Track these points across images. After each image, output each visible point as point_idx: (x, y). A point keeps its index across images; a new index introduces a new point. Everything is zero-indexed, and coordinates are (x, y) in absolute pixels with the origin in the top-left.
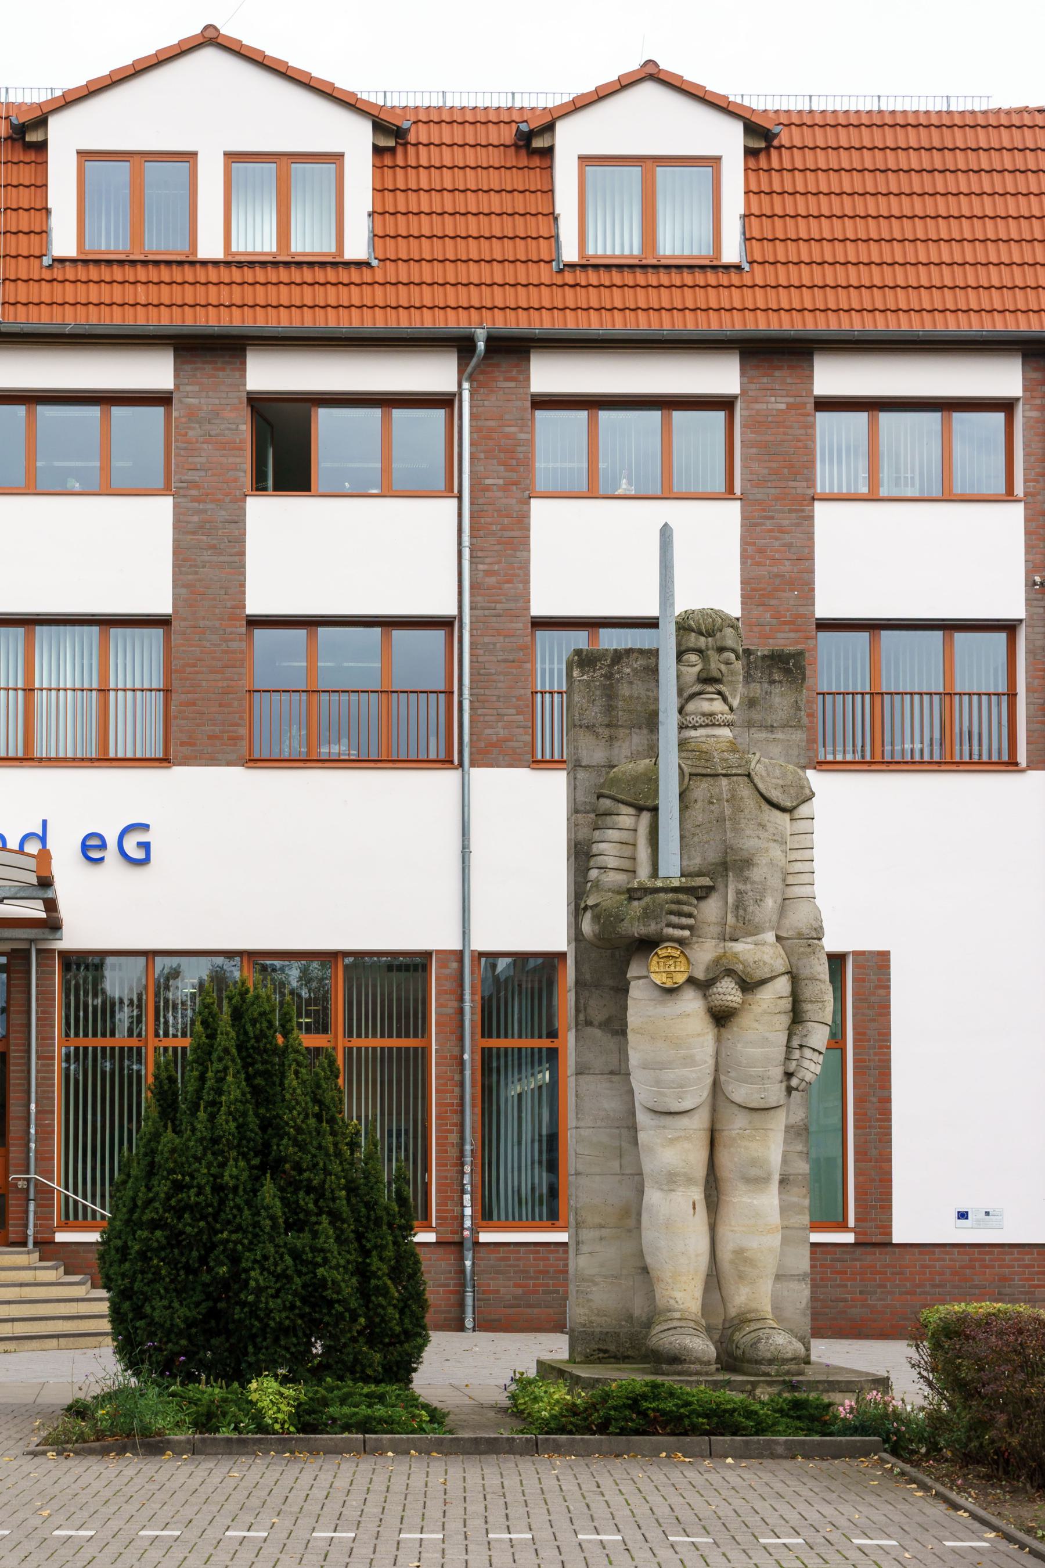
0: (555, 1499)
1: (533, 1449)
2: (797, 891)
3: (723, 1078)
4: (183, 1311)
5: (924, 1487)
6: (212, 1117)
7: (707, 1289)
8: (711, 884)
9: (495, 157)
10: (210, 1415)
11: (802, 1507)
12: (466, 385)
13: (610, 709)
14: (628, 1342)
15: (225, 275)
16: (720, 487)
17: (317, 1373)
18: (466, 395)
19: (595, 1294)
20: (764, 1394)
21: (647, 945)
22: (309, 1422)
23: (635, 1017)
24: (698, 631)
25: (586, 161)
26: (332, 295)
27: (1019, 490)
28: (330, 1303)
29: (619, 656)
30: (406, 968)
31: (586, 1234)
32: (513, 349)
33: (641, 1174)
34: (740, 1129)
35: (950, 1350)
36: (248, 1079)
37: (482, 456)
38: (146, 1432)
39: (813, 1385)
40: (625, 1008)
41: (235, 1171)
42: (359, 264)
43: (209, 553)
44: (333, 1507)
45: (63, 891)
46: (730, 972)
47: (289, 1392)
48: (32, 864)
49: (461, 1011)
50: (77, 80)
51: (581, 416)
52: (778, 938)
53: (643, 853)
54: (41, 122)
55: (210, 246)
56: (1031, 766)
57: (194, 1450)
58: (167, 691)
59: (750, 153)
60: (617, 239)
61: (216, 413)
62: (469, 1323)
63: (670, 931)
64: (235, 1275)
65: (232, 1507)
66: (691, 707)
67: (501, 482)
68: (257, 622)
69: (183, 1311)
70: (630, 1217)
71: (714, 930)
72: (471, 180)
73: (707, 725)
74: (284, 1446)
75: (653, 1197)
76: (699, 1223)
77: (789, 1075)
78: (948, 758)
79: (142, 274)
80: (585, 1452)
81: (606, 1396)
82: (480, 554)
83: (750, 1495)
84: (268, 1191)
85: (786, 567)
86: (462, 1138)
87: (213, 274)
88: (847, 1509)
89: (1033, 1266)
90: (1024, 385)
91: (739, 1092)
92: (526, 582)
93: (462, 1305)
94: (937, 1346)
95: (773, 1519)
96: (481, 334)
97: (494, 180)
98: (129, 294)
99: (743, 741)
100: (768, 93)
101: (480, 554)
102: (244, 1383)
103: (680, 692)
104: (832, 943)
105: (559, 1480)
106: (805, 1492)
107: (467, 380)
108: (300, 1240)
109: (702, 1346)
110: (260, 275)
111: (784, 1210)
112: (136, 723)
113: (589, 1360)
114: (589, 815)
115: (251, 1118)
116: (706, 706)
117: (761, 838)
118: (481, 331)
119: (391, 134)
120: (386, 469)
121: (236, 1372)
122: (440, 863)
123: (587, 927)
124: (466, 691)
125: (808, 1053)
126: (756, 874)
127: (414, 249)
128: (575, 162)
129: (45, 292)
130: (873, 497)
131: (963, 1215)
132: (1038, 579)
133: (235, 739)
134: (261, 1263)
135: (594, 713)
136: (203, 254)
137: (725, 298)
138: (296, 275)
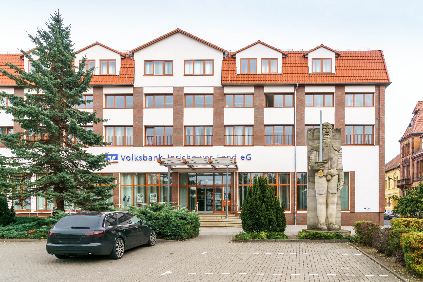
0: (301, 248)
1: (299, 241)
4: (252, 222)
5: (354, 247)
6: (256, 195)
7: (326, 219)
9: (300, 58)
10: (255, 237)
11: (336, 250)
13: (313, 137)
14: (315, 227)
15: (261, 76)
16: (332, 105)
17: (270, 231)
19: (310, 220)
20: (333, 233)
21: (318, 171)
22: (269, 238)
24: (325, 126)
25: (313, 59)
26: (276, 79)
27: (375, 105)
28: (272, 221)
29: (314, 129)
30: (287, 174)
31: (309, 211)
32: (302, 86)
35: (358, 227)
36: (261, 190)
38: (245, 239)
39: (340, 232)
41: (259, 203)
42: (280, 74)
43: (259, 115)
44: (269, 250)
45: (238, 164)
46: (329, 174)
47: (266, 234)
48: (233, 160)
50: (240, 48)
51: (363, 95)
53: (317, 157)
54: (235, 55)
55: (259, 72)
57: (252, 242)
58: (253, 135)
59: (336, 57)
60: (317, 70)
61: (260, 96)
64: (259, 217)
65: (255, 250)
68: (265, 126)
69: (252, 222)
71: (327, 168)
72: (296, 62)
74: (265, 241)
75: (318, 206)
76: (325, 210)
77: (338, 189)
78: (364, 144)
79: (249, 76)
80: (307, 242)
81: (310, 234)
83: (329, 248)
84: (263, 205)
85: (341, 117)
87: (259, 76)
88: (342, 250)
91: (331, 191)
92: (304, 119)
93: (294, 221)
94: (356, 227)
95: (331, 251)
96: (298, 84)
97: (300, 62)
98: (248, 79)
99: (332, 141)
100: (339, 48)
102: (260, 233)
104: (345, 170)
105: (303, 245)
106: (337, 247)
108: (268, 212)
109: (325, 227)
110: (266, 76)
111: (337, 208)
112: (249, 140)
113: (309, 229)
114: (310, 152)
115: (261, 195)
116: (326, 136)
117: (335, 155)
119: (285, 56)
120: (244, 104)
121: (259, 231)
122: (291, 160)
123: (309, 168)
126: (333, 160)
127: (288, 72)
128: (261, 59)
129: (236, 79)
130: (354, 107)
131: (365, 209)
133: (262, 142)
134: (262, 216)
135: (311, 138)
136: (258, 73)
137: (333, 78)
138: (271, 76)
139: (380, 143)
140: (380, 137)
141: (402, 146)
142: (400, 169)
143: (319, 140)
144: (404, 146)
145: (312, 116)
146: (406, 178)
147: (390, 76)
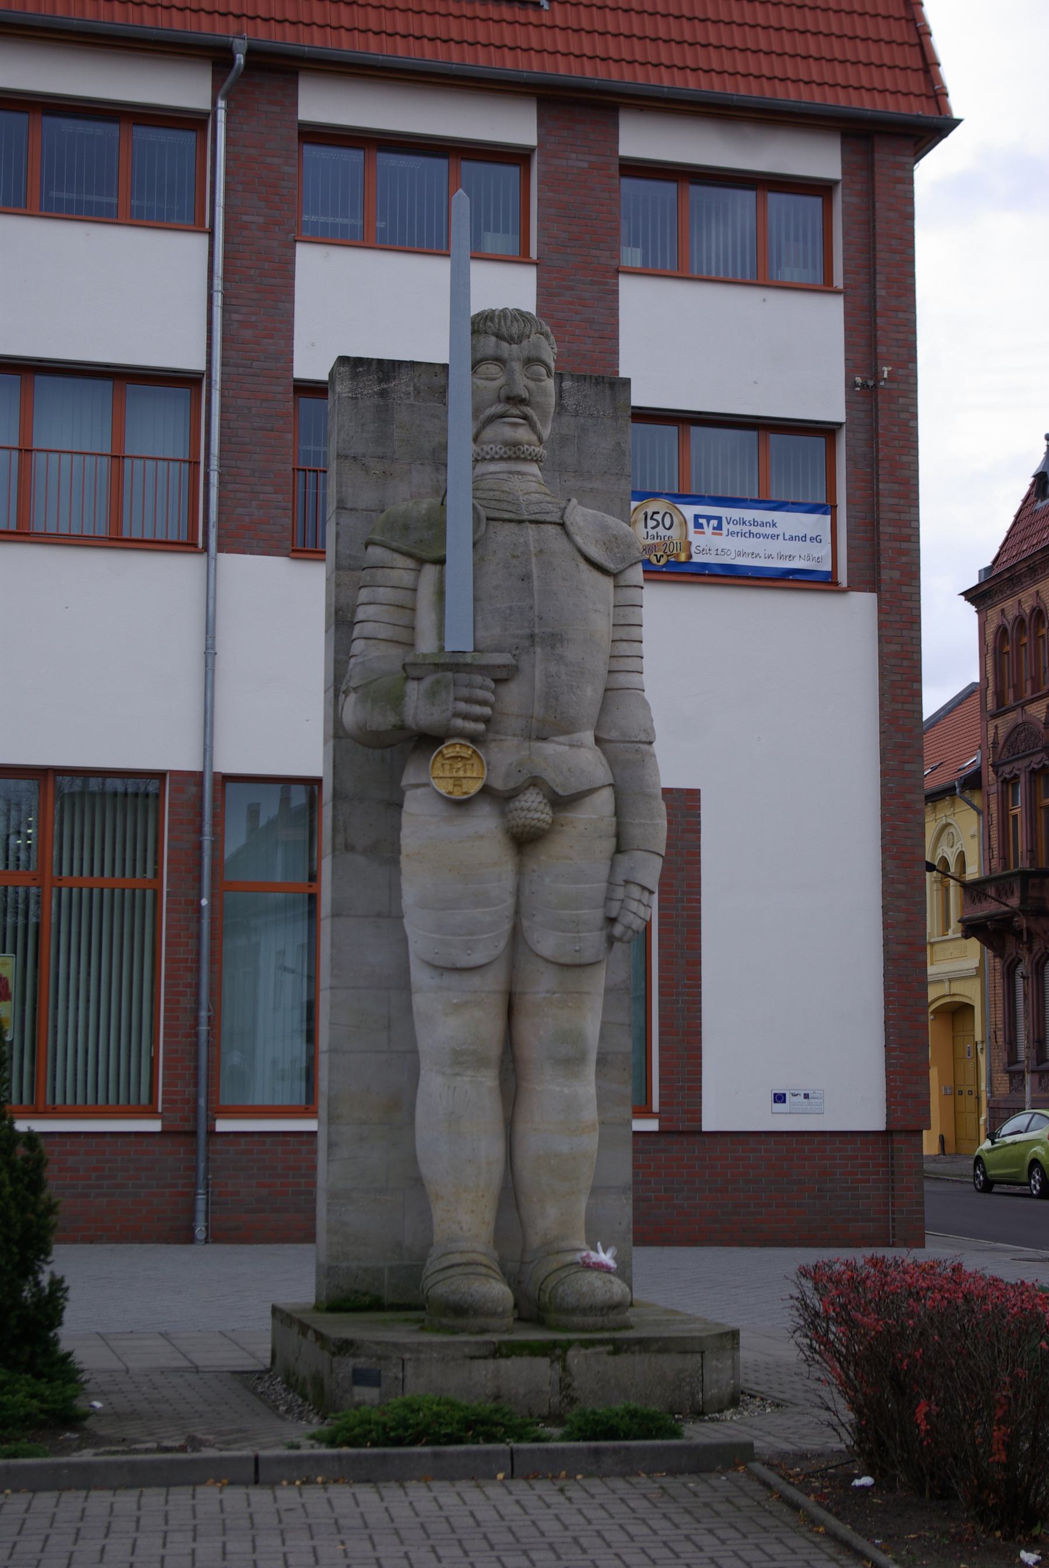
2: (623, 680)
3: (525, 923)
8: (514, 662)
12: (221, 103)
18: (221, 115)
21: (428, 741)
23: (410, 839)
27: (839, 281)
32: (277, 69)
33: (415, 1051)
34: (548, 992)
37: (240, 188)
40: (397, 828)
46: (535, 782)
49: (199, 846)
52: (598, 741)
56: (852, 587)
62: (200, 1231)
63: (459, 723)
66: (488, 433)
67: (261, 220)
70: (398, 1109)
73: (509, 458)
82: (234, 301)
86: (197, 1002)
89: (856, 1157)
90: (843, 168)
91: (546, 942)
93: (192, 1210)
101: (234, 301)
103: (476, 412)
107: (222, 99)
118: (241, 41)
123: (352, 713)
124: (214, 462)
125: (636, 892)
131: (779, 1098)
132: (859, 380)
139: (885, 574)
140: (886, 529)
141: (991, 629)
142: (977, 799)
143: (440, 464)
144: (1002, 632)
145: (365, 304)
146: (1024, 864)
147: (952, 73)
